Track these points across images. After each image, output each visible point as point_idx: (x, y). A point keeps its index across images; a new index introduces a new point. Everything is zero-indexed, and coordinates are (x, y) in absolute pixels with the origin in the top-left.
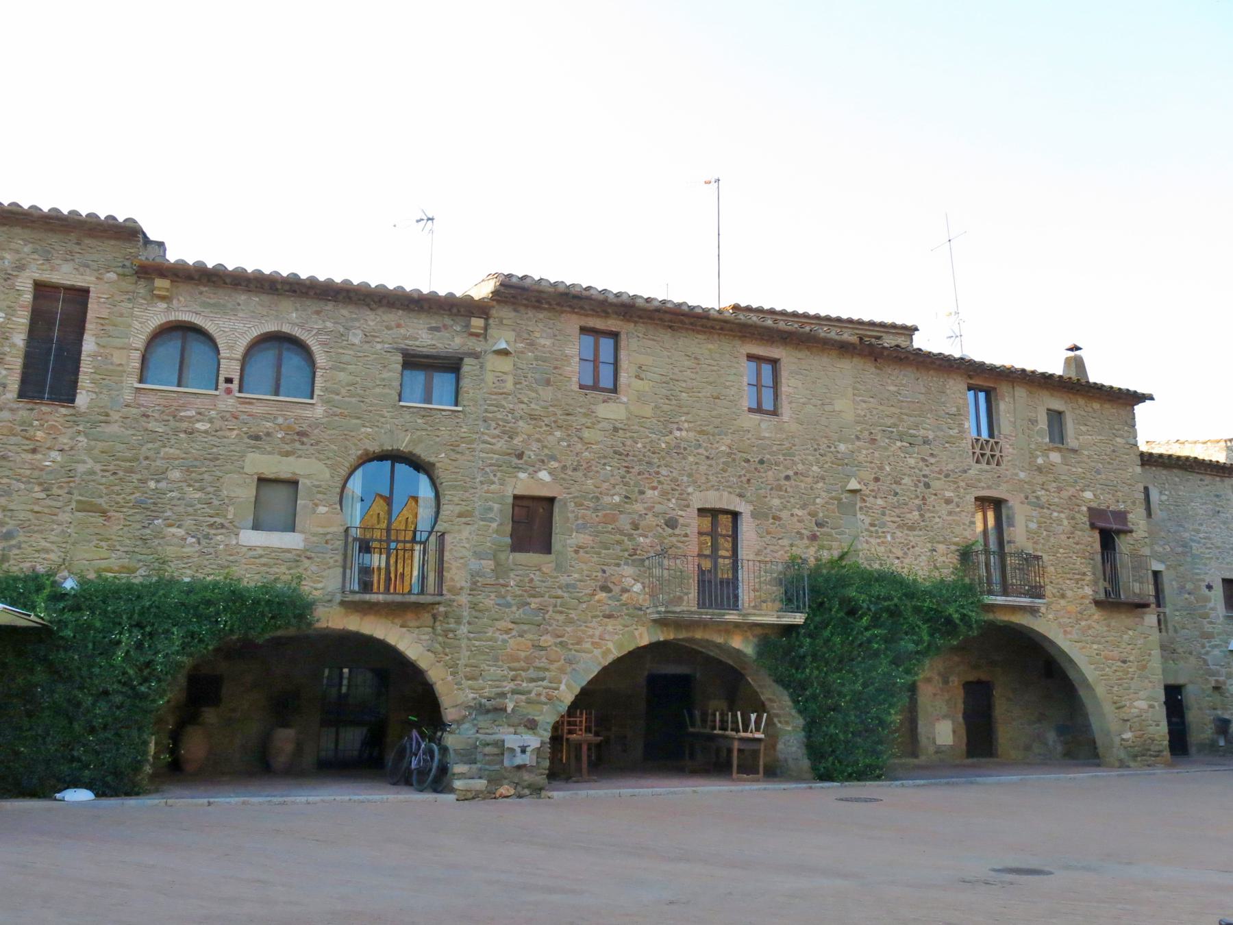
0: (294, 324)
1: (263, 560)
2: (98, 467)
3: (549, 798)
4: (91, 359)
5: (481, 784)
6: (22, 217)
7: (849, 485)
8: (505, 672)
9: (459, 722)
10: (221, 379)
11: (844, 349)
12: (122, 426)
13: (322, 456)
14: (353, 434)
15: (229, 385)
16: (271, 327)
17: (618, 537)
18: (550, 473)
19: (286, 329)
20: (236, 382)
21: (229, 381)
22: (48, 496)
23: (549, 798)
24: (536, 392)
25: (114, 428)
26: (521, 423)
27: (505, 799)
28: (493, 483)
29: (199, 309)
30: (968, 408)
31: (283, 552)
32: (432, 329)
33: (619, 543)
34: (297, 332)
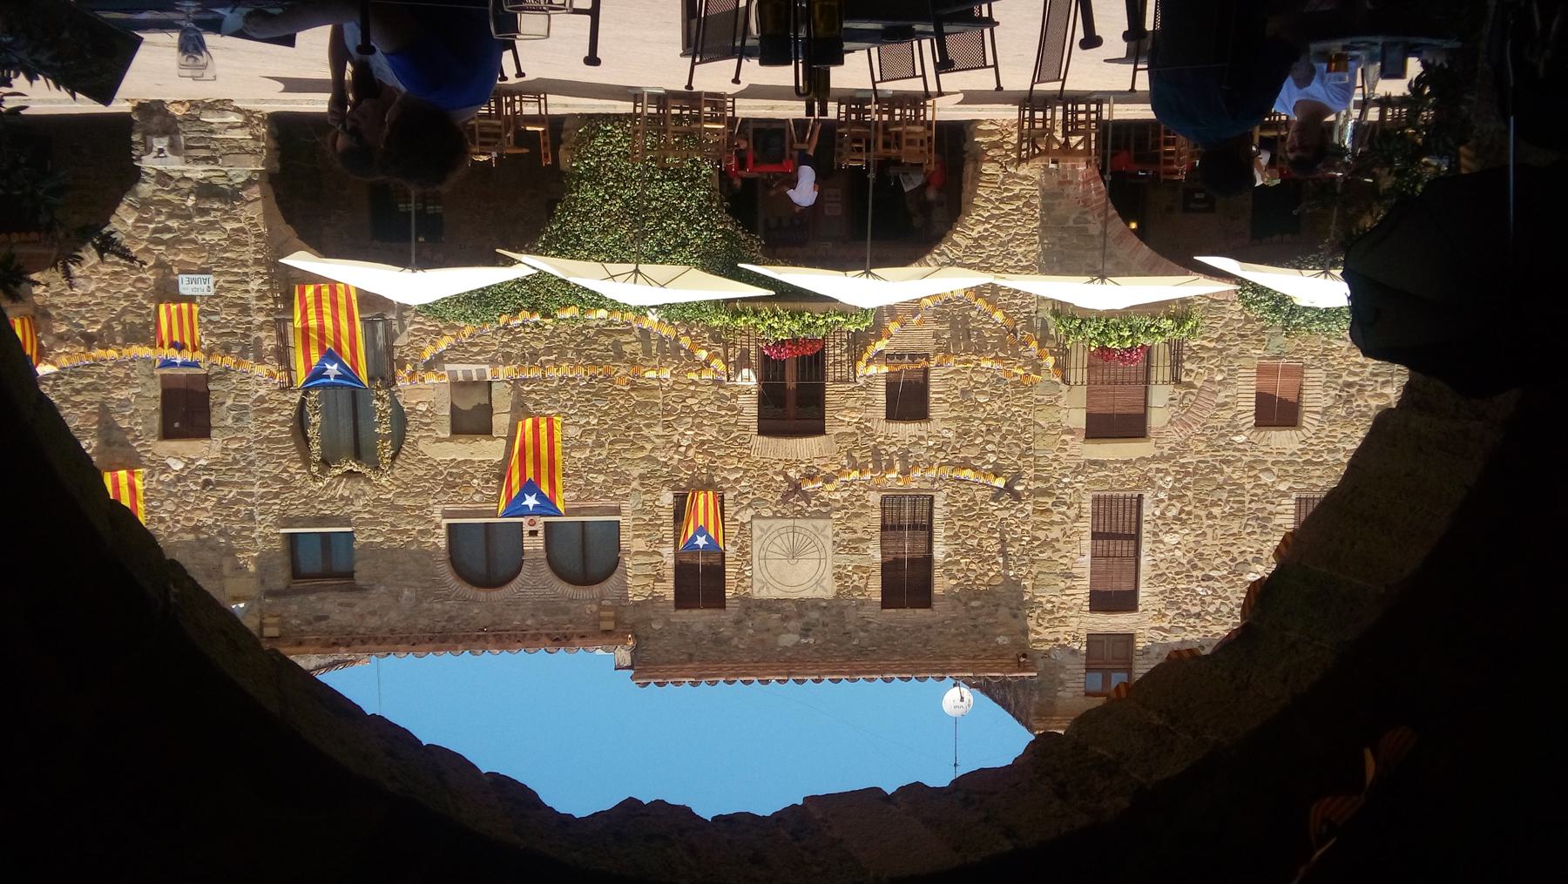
0: (475, 601)
1: (475, 349)
2: (645, 432)
3: (127, 100)
4: (664, 540)
5: (210, 118)
6: (781, 671)
7: (1151, 118)
8: (200, 237)
9: (249, 183)
10: (541, 534)
11: (487, 548)
12: (628, 475)
13: (429, 462)
14: (399, 490)
15: (533, 528)
16: (497, 595)
17: (79, 399)
18: (169, 467)
19: (482, 594)
20: (526, 533)
21: (533, 533)
22: (684, 401)
23: (127, 100)
24: (1332, 355)
25: (636, 472)
26: (210, 522)
27: (179, 100)
28: (235, 450)
29: (573, 605)
30: (1000, 289)
31: (458, 359)
32: (325, 618)
33: (78, 392)
34: (469, 591)
